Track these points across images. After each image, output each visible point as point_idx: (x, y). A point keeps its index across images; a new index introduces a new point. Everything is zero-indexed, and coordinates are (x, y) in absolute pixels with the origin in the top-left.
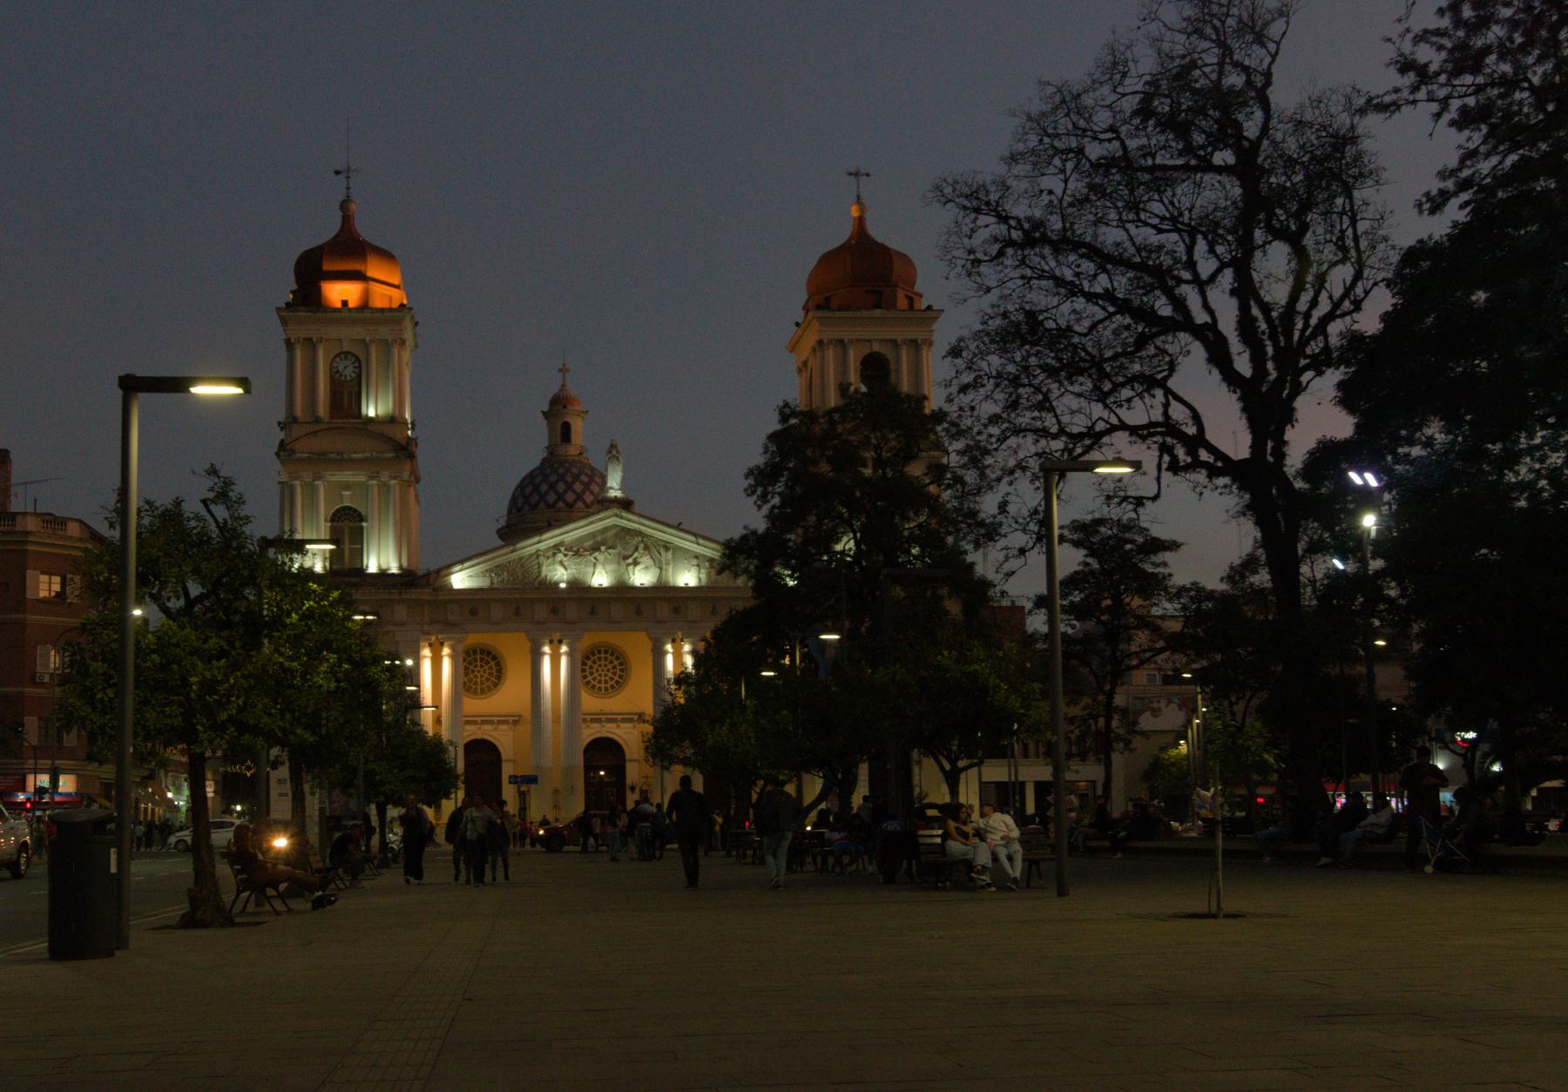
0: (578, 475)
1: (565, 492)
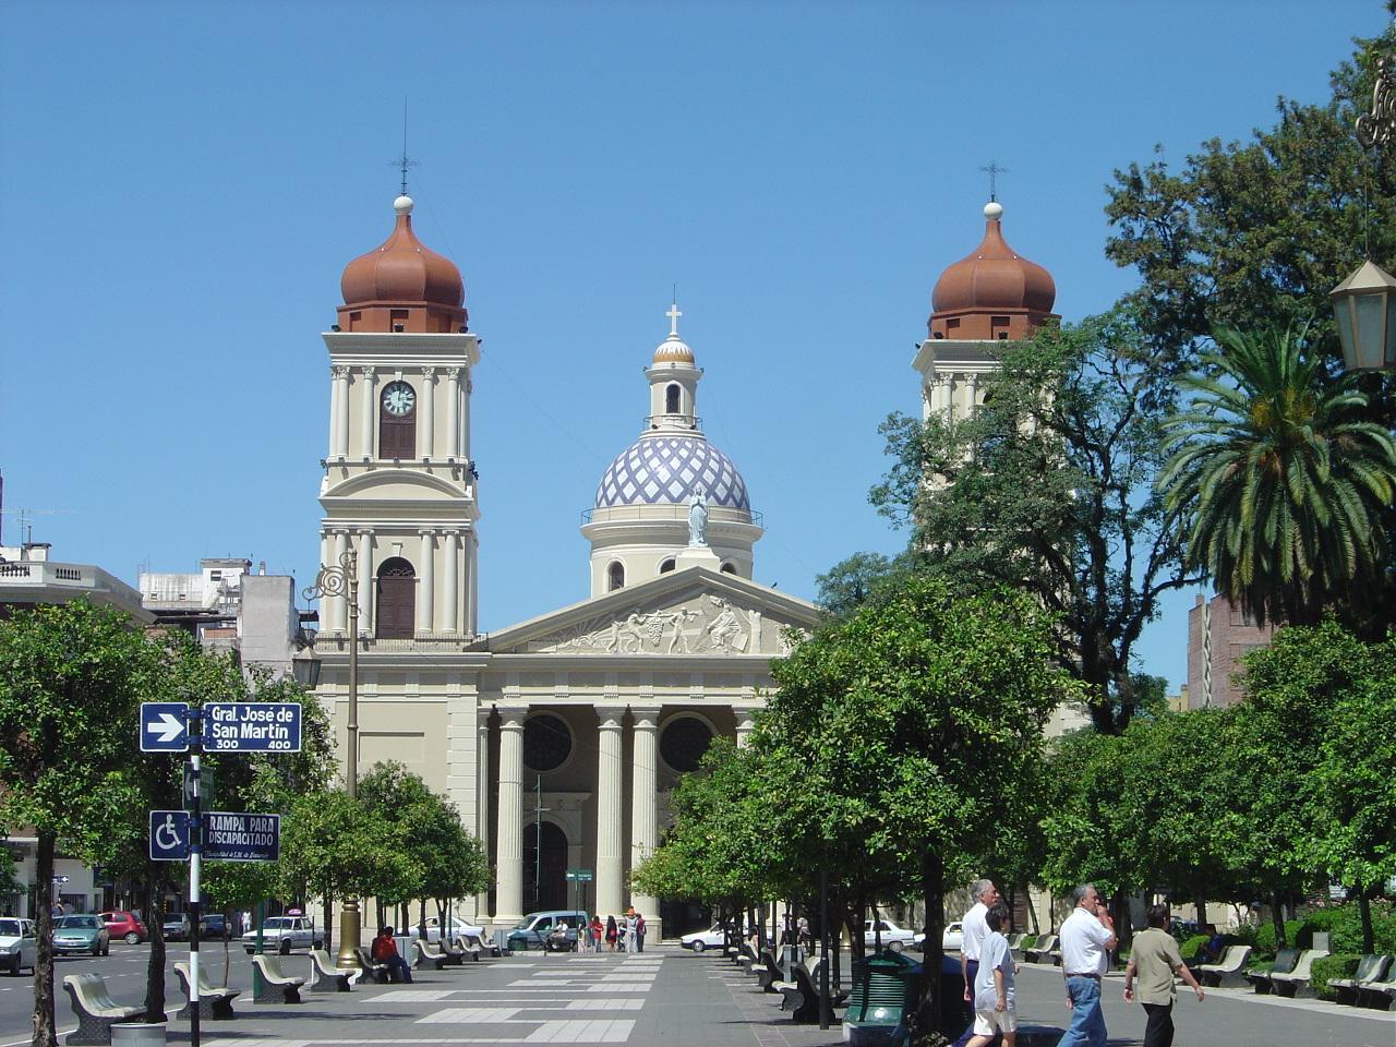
0: (689, 459)
1: (670, 482)
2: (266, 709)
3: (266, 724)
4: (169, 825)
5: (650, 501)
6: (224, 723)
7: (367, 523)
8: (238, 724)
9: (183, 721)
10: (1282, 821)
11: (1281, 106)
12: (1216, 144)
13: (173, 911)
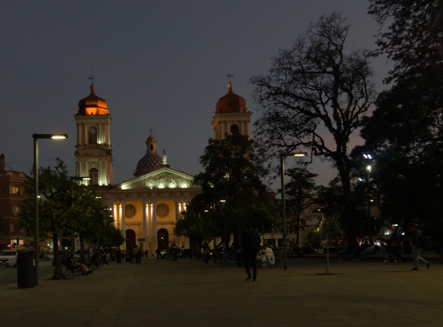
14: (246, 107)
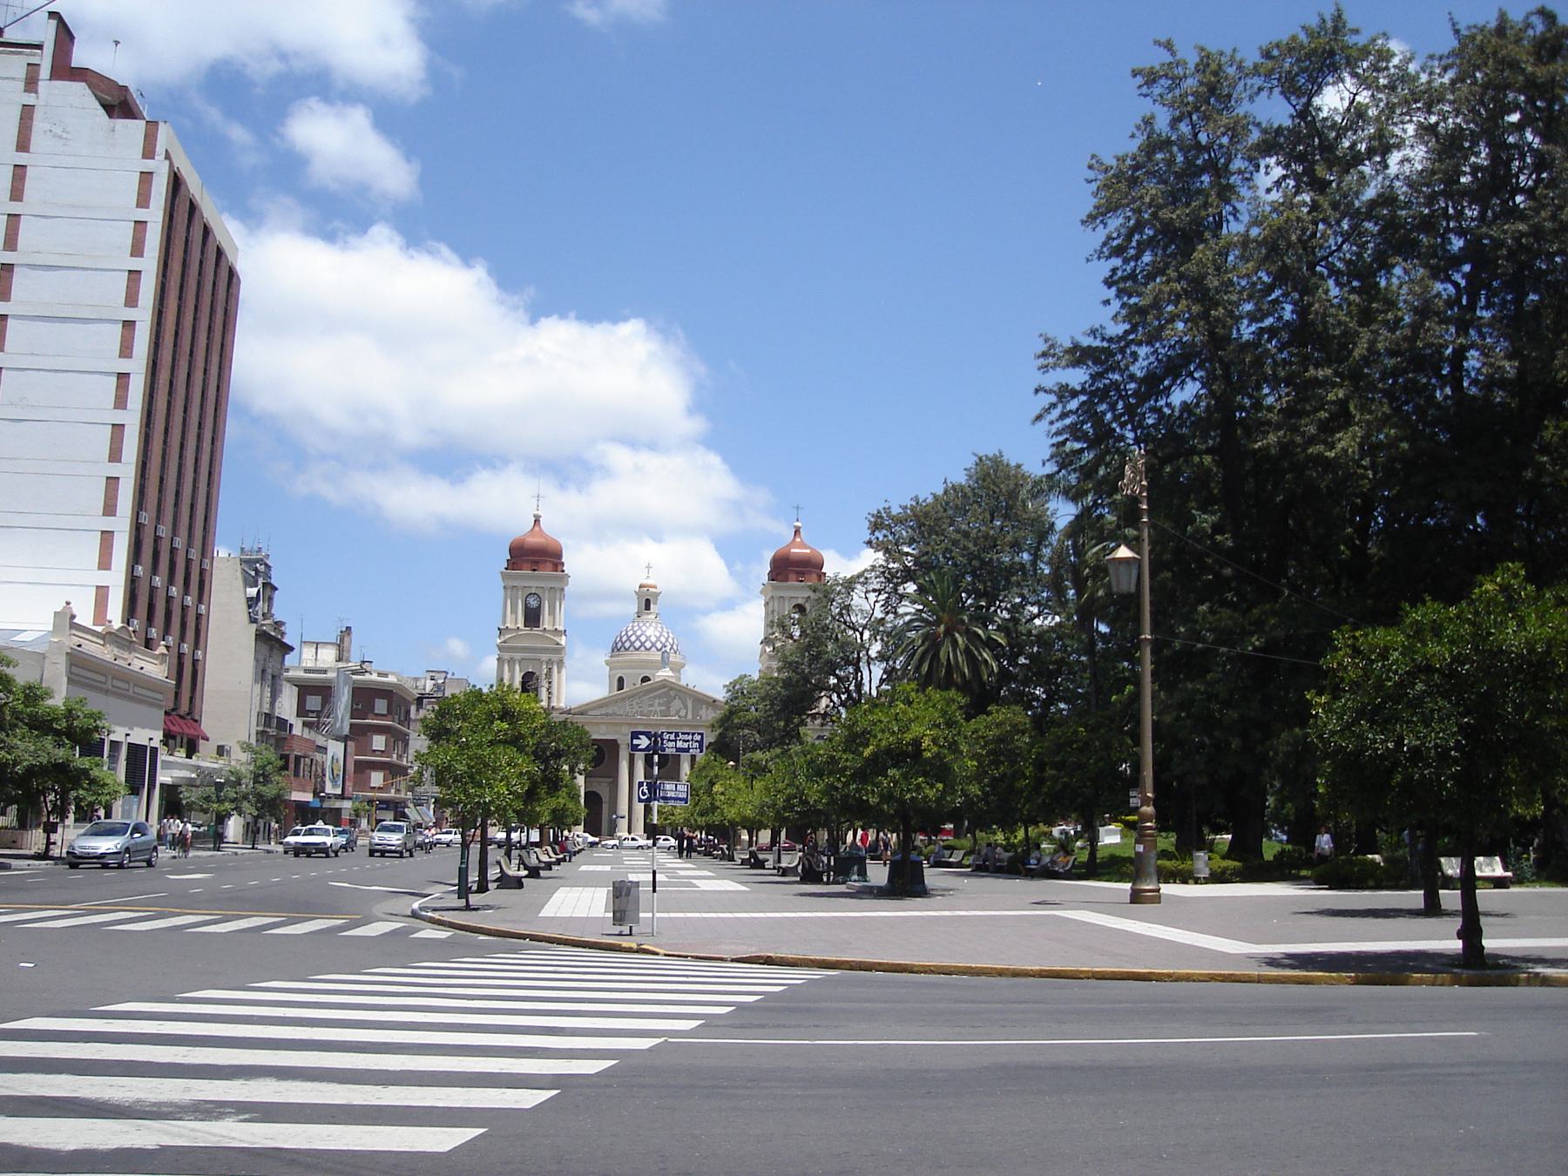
2: (688, 734)
3: (688, 741)
4: (645, 787)
5: (637, 649)
6: (669, 740)
7: (518, 656)
8: (676, 741)
9: (650, 739)
10: (675, 776)
11: (945, 482)
12: (916, 499)
13: (110, 818)
14: (823, 571)
